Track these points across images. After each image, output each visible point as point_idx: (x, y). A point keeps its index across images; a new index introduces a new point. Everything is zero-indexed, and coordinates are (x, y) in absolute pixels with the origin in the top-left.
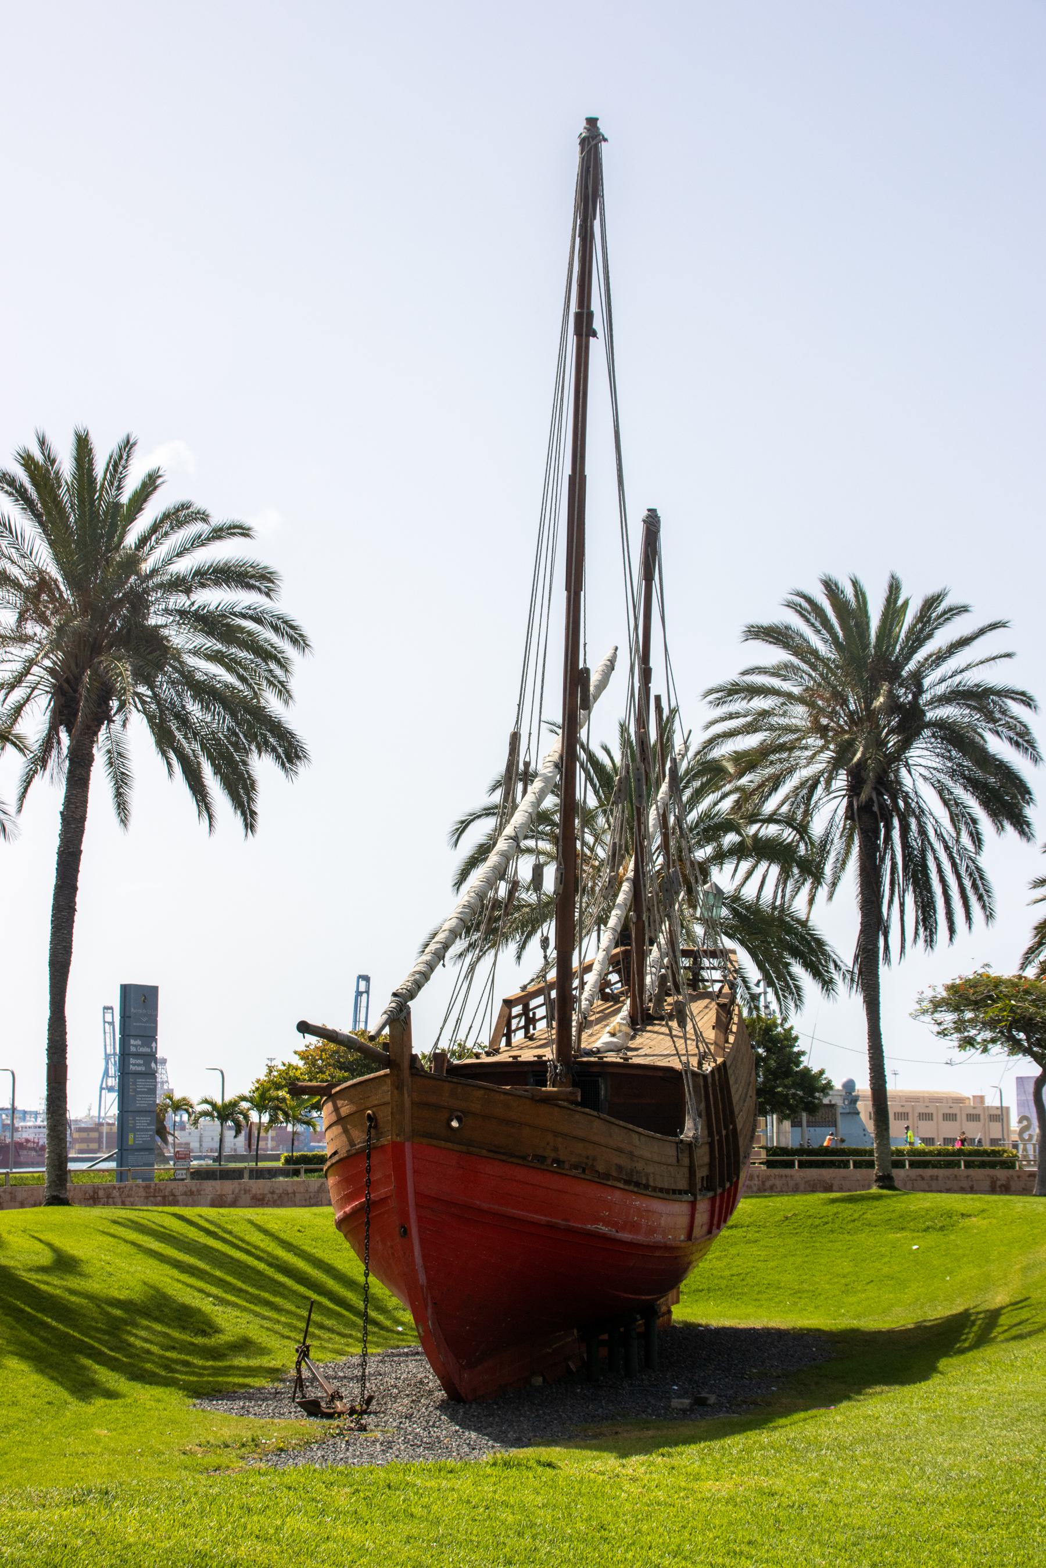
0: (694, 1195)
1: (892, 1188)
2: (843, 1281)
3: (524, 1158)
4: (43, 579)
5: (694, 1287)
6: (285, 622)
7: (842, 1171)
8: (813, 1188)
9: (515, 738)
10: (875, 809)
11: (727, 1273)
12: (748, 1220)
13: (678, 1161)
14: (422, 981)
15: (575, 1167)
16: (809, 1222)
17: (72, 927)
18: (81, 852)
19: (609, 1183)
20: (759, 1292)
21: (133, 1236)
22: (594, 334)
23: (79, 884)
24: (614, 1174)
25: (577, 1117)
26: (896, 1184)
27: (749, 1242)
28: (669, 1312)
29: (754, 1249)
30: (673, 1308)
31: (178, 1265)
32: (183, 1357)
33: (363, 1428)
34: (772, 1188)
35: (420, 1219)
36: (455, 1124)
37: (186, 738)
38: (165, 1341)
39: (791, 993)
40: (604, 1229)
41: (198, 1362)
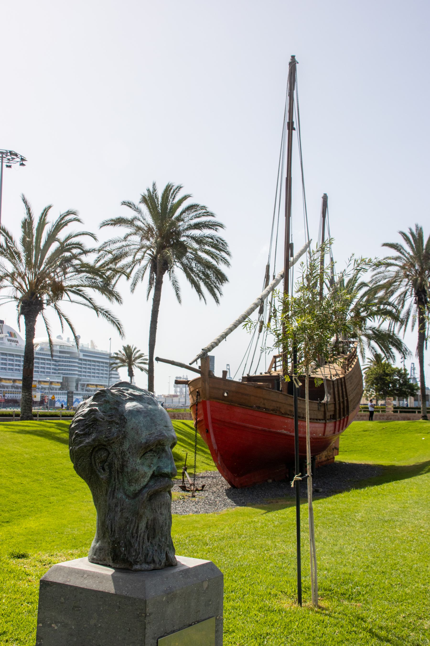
0: (326, 421)
1: (427, 419)
2: (398, 449)
3: (252, 407)
4: (150, 227)
5: (350, 450)
6: (220, 239)
7: (414, 414)
8: (404, 419)
9: (268, 267)
10: (423, 300)
11: (362, 445)
12: (371, 429)
13: (318, 409)
14: (215, 345)
16: (391, 430)
17: (155, 334)
18: (158, 311)
19: (286, 416)
20: (371, 452)
22: (294, 129)
23: (158, 321)
24: (288, 413)
25: (272, 393)
26: (428, 418)
27: (370, 436)
28: (334, 458)
29: (372, 438)
30: (335, 457)
33: (194, 496)
34: (391, 419)
35: (214, 427)
36: (226, 395)
37: (195, 276)
39: (392, 358)
40: (285, 432)
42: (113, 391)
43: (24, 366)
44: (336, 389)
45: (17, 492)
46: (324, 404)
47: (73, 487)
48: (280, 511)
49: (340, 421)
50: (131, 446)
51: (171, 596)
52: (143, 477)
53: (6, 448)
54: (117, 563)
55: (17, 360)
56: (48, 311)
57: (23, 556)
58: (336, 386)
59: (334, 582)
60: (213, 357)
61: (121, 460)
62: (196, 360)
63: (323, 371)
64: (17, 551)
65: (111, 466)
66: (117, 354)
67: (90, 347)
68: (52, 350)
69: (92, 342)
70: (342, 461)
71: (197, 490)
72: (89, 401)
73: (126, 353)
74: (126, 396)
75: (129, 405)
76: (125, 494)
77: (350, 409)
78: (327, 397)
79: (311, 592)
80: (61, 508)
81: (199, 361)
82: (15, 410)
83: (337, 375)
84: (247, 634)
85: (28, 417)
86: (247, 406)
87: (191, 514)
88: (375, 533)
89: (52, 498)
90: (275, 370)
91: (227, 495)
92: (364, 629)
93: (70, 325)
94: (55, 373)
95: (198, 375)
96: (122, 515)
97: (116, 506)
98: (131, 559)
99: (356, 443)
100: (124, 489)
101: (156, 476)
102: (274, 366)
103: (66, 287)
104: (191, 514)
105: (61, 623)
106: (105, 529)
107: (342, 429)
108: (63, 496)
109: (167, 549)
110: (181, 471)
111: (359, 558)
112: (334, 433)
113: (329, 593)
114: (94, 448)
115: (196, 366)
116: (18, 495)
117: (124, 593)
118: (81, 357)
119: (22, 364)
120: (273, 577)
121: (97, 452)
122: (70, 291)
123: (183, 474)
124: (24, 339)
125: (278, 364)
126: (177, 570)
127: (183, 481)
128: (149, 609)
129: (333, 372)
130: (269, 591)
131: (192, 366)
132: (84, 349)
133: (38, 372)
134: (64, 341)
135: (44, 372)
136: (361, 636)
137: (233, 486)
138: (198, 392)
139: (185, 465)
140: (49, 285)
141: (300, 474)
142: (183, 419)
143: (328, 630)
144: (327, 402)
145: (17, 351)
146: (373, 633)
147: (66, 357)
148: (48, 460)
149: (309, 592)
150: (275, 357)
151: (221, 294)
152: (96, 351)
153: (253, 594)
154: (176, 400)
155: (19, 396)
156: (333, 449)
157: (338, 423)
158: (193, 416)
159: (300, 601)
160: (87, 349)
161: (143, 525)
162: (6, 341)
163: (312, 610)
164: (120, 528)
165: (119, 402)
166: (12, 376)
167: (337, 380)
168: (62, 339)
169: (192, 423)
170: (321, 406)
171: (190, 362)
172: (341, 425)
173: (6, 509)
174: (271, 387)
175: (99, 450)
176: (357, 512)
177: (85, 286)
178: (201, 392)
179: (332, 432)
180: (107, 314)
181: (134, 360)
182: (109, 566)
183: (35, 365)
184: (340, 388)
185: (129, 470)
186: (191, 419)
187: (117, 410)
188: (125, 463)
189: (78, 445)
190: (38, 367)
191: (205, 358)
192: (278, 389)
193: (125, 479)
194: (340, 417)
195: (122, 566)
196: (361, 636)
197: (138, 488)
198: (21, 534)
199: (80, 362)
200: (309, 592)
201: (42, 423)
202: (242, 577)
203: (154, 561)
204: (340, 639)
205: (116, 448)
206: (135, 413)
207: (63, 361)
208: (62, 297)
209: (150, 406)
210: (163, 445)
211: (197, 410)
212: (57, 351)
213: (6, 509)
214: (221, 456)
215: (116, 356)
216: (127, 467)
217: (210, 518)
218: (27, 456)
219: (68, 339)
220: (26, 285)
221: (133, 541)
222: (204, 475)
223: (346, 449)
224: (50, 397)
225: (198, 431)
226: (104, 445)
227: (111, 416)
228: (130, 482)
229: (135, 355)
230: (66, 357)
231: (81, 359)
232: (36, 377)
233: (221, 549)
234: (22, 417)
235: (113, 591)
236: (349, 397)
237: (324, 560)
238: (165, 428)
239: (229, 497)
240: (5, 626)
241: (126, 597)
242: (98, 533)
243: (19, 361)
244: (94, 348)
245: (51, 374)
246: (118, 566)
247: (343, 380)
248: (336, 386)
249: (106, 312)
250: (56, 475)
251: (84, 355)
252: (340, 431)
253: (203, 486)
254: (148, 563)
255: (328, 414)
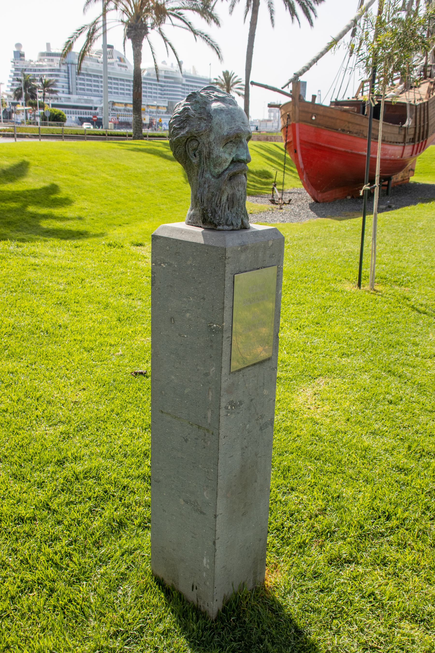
3: (337, 130)
15: (356, 133)
21: (258, 150)
25: (357, 117)
28: (409, 179)
31: (268, 159)
32: (255, 184)
35: (301, 148)
36: (314, 118)
38: (252, 179)
41: (259, 186)
42: (202, 93)
43: (134, 91)
44: (418, 114)
45: (133, 200)
46: (405, 128)
47: (179, 198)
48: (352, 220)
49: (418, 145)
50: (215, 137)
51: (244, 248)
52: (225, 162)
53: (122, 164)
54: (206, 225)
55: (127, 85)
56: (153, 35)
57: (141, 245)
58: (418, 110)
59: (389, 273)
60: (305, 83)
61: (208, 149)
62: (288, 84)
63: (407, 95)
64: (136, 241)
65: (200, 153)
66: (216, 79)
67: (192, 73)
68: (158, 76)
69: (193, 67)
70: (417, 181)
71: (284, 203)
72: (183, 102)
73: (225, 78)
74: (212, 98)
75: (215, 105)
76: (211, 175)
77: (430, 133)
78: (409, 121)
79: (369, 280)
80: (170, 214)
81: (291, 85)
82: (128, 131)
83: (421, 99)
84: (314, 306)
85: (139, 137)
86: (333, 129)
87: (278, 223)
88: (432, 238)
89: (162, 206)
90: (362, 95)
91: (311, 208)
92: (408, 305)
93: (174, 52)
94: (161, 98)
95: (289, 99)
96: (209, 190)
97: (205, 183)
98: (216, 222)
99: (431, 165)
100: (210, 171)
101: (235, 162)
102: (361, 91)
103: (169, 10)
104: (278, 223)
105: (167, 263)
106: (197, 200)
107: (420, 152)
108: (171, 205)
109: (242, 216)
110: (271, 187)
111: (413, 256)
112: (411, 155)
113: (384, 280)
114: (188, 139)
115: (288, 90)
116: (134, 203)
117: (211, 244)
118: (184, 82)
119: (132, 88)
120: (339, 268)
121: (190, 142)
122: (172, 14)
123: (273, 189)
124: (132, 64)
125: (365, 89)
126: (249, 231)
127: (273, 196)
128: (228, 254)
129: (418, 97)
130: (335, 277)
131: (284, 90)
132: (187, 74)
133: (146, 96)
134: (168, 67)
135: (151, 97)
136: (404, 310)
137: (316, 201)
138: (288, 115)
139: (275, 182)
140: (153, 8)
141: (369, 184)
142: (275, 141)
143: (378, 306)
144: (408, 126)
145: (127, 76)
146: (414, 308)
147: (170, 83)
148: (157, 174)
149: (367, 280)
150: (363, 82)
151: (316, 16)
152: (197, 76)
153: (322, 279)
154: (269, 124)
155: (131, 119)
156: (409, 171)
157: (416, 146)
158: (284, 138)
159: (359, 285)
160: (189, 75)
161: (224, 198)
162: (116, 66)
163: (368, 292)
164: (207, 200)
165: (206, 103)
166: (123, 100)
167: (420, 104)
168: (166, 64)
169: (282, 145)
170: (401, 130)
171: (283, 86)
172: (419, 148)
173: (125, 214)
174: (356, 111)
175: (192, 140)
176: (420, 221)
177: (186, 9)
178: (291, 115)
179: (410, 154)
180: (207, 38)
181: (232, 86)
182: (200, 227)
183: (143, 89)
184: (422, 113)
185: (214, 157)
186: (281, 141)
187: (205, 108)
188: (211, 151)
189: (176, 136)
190: (146, 92)
191: (297, 83)
192: (363, 113)
193: (211, 164)
194: (419, 140)
195: (210, 227)
196: (404, 310)
197: (221, 170)
198: (139, 234)
199: (183, 87)
200: (367, 280)
201: (151, 142)
202: (315, 267)
203: (232, 224)
204: (387, 311)
205: (204, 139)
206: (219, 111)
207: (167, 86)
208: (165, 20)
209: (231, 106)
210: (240, 137)
211: (287, 132)
212: (162, 76)
213: (125, 214)
214: (307, 174)
215: (215, 81)
216: (212, 154)
217: (294, 227)
218: (140, 171)
219: (172, 64)
220: (132, 9)
221: (217, 209)
222: (291, 191)
223: (421, 171)
224: (158, 120)
225: (287, 151)
226: (196, 137)
227: (200, 114)
228: (215, 166)
229: (233, 80)
230: (170, 83)
231: (184, 85)
232: (145, 101)
233: (300, 247)
234: (134, 137)
235: (203, 242)
236: (430, 121)
237: (384, 257)
238: (242, 124)
239: (312, 210)
240: (131, 290)
241: (212, 246)
242: (192, 204)
243: (129, 86)
244: (196, 74)
245: (158, 99)
246: (206, 227)
247: (426, 105)
248: (418, 110)
249: (206, 36)
250: (165, 187)
251: (187, 81)
252: (418, 154)
253: (290, 200)
254: (228, 225)
255: (408, 138)
